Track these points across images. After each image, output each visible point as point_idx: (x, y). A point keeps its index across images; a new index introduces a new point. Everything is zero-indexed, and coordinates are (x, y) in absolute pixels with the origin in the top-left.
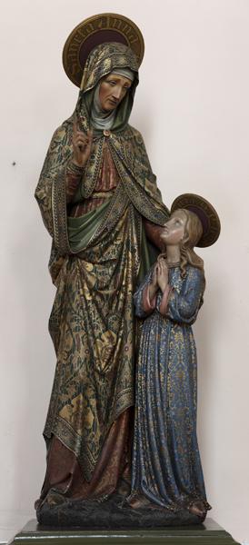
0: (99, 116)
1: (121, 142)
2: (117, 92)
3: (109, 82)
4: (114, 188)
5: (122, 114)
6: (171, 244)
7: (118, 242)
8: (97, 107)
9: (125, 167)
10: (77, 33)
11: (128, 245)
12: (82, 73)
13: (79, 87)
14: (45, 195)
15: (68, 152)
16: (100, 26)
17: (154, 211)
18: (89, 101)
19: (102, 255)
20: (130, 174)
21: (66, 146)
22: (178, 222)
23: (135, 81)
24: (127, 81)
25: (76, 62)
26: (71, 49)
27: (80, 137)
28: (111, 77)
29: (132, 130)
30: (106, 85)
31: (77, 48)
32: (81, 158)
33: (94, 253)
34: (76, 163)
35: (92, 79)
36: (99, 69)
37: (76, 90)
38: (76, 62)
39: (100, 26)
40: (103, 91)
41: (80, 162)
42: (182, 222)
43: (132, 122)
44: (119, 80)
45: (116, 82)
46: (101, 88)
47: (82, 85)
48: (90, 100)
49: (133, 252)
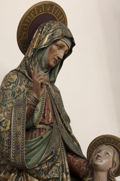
3: (57, 45)
4: (52, 123)
6: (102, 171)
7: (58, 165)
10: (34, 10)
11: (63, 168)
12: (27, 50)
13: (24, 55)
14: (4, 118)
15: (20, 90)
16: (48, 10)
17: (75, 146)
18: (40, 56)
19: (47, 174)
20: (60, 116)
21: (18, 86)
22: (108, 154)
23: (70, 52)
25: (26, 31)
26: (26, 20)
28: (59, 42)
30: (54, 47)
31: (30, 20)
33: (43, 170)
34: (36, 96)
35: (46, 40)
36: (53, 35)
37: (22, 56)
38: (26, 31)
39: (48, 10)
40: (52, 51)
42: (110, 154)
43: (56, 84)
44: (64, 46)
45: (61, 47)
46: (51, 49)
47: (26, 54)
48: (41, 55)
49: (66, 174)
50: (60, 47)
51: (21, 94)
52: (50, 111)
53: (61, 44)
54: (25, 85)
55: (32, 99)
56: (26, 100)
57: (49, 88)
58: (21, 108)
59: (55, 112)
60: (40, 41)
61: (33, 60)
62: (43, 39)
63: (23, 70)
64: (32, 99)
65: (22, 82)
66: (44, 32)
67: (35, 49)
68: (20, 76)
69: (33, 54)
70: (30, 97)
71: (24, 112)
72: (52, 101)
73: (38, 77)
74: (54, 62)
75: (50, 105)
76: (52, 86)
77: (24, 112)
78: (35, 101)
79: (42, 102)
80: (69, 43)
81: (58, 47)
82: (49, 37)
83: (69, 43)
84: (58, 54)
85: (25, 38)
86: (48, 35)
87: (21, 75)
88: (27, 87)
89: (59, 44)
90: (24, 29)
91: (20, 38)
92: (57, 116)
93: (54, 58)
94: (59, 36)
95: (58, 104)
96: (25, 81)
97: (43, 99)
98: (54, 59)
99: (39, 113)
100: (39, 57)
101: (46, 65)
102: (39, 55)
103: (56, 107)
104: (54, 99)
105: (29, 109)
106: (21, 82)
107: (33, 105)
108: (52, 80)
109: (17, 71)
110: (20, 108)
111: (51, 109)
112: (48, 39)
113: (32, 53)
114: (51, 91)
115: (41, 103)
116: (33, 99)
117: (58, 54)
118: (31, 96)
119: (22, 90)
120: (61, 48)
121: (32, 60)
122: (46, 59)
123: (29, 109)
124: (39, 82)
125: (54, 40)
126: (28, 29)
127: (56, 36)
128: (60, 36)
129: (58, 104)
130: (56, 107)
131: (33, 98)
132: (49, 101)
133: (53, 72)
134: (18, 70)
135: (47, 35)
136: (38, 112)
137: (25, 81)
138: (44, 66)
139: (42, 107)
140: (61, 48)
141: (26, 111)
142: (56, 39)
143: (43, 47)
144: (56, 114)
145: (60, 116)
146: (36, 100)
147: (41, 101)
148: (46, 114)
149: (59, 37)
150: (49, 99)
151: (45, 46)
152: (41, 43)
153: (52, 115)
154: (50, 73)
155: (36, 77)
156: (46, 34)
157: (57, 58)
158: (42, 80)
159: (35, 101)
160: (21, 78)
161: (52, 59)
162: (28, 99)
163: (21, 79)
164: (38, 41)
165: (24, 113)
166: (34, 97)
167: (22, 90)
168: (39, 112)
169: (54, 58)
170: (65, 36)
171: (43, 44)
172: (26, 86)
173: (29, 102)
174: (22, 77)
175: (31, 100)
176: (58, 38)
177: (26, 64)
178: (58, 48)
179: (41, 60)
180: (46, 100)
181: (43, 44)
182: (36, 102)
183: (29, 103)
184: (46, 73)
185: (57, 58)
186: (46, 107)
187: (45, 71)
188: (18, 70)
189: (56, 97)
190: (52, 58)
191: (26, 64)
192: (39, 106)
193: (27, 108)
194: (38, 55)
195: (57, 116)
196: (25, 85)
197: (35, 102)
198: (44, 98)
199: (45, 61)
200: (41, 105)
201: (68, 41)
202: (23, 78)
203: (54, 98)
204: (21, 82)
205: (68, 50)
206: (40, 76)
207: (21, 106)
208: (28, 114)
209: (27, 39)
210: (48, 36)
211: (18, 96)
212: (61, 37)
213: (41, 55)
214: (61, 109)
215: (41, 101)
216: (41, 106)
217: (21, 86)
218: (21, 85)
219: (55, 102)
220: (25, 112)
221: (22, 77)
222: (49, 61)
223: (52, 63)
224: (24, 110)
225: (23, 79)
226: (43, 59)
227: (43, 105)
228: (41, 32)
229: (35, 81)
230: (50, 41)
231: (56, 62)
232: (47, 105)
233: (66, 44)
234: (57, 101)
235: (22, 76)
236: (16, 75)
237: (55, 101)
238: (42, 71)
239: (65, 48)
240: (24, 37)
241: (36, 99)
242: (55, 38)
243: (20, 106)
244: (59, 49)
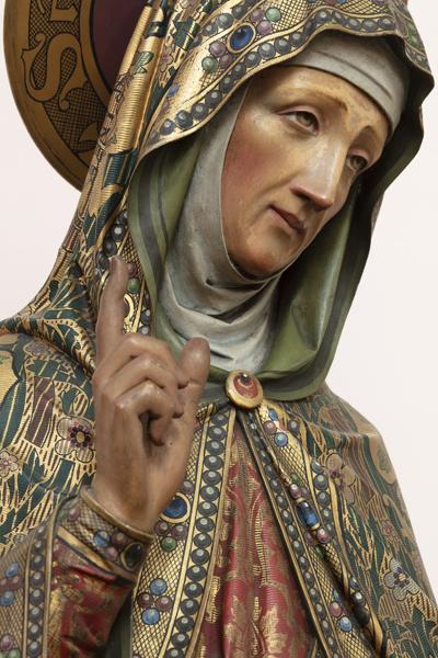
0: (201, 295)
1: (311, 447)
2: (322, 166)
3: (282, 110)
5: (310, 315)
8: (198, 251)
9: (338, 582)
15: (32, 471)
18: (161, 202)
20: (361, 622)
23: (405, 137)
24: (370, 117)
25: (73, 28)
27: (146, 364)
28: (298, 85)
29: (344, 415)
30: (264, 124)
32: (143, 485)
34: (115, 511)
35: (192, 88)
36: (240, 36)
38: (73, 28)
40: (245, 156)
41: (137, 507)
43: (343, 379)
44: (340, 105)
45: (314, 118)
47: (86, 189)
48: (170, 199)
50: (307, 116)
51: (37, 497)
52: (271, 597)
53: (312, 93)
54: (74, 432)
55: (89, 536)
56: (45, 546)
57: (257, 433)
58: (17, 606)
59: (316, 599)
60: (160, 92)
61: (121, 237)
62: (175, 73)
63: (53, 323)
64: (89, 536)
65: (49, 413)
66: (182, 27)
67: (128, 154)
68: (39, 364)
69: (116, 199)
70: (73, 520)
71: (34, 630)
72: (289, 522)
73: (118, 371)
74: (280, 234)
75: (266, 552)
76: (280, 412)
77: (34, 630)
78: (111, 543)
79: (195, 540)
80: (381, 80)
81: (293, 118)
82: (213, 57)
83: (390, 91)
84: (294, 175)
85: (77, 80)
86: (207, 42)
87: (49, 355)
88: (88, 440)
89: (292, 98)
90: (57, 15)
91: (37, 88)
92: (327, 633)
93: (272, 207)
94: (282, 43)
95: (345, 535)
96: (69, 398)
97: (206, 514)
98: (270, 214)
99: (177, 621)
100: (154, 213)
101: (220, 268)
102: (153, 196)
103: (326, 559)
104: (299, 509)
105: (79, 609)
106: (42, 406)
107: (95, 577)
108: (292, 356)
109: (22, 330)
110: (8, 604)
111: (271, 583)
112: (208, 71)
113: (110, 190)
114: (279, 445)
115: (190, 546)
116: (96, 534)
117: (294, 175)
118: (78, 515)
119: (50, 472)
120: (316, 127)
121: (110, 237)
122: (214, 218)
123: (79, 609)
124: (128, 404)
125: (251, 72)
126: (85, 14)
127: (264, 49)
128: (291, 42)
129: (345, 535)
130: (326, 559)
131: (99, 525)
132: (260, 523)
133: (298, 300)
134: (27, 327)
135: (199, 43)
136: (165, 615)
137: (69, 398)
138: (204, 270)
139: (195, 578)
140: (316, 127)
141: (52, 627)
142: (263, 65)
143: (177, 134)
144: (322, 616)
145: (361, 622)
146: (120, 537)
147: (193, 531)
148: (229, 628)
149: (285, 51)
150: (262, 507)
151: (185, 125)
152: (164, 111)
153: (281, 628)
154: (277, 318)
155: (110, 369)
156: (194, 34)
157: (292, 206)
158: (148, 389)
159: (111, 543)
160: (45, 383)
161: (257, 216)
162: (62, 532)
163: (39, 391)
164: (142, 98)
165: (33, 637)
166: (100, 515)
167: (50, 472)
168: (177, 613)
169: (272, 207)
170: (329, 33)
171: (172, 116)
172: (80, 439)
173: (71, 559)
174: (48, 372)
175: (83, 540)
176: (279, 59)
177: (77, 270)
178: (291, 125)
179: (175, 232)
180: (230, 520)
181: (172, 116)
182: (118, 547)
183: (69, 562)
184: (238, 322)
185: (292, 206)
186: (234, 574)
187: (223, 307)
188: (27, 327)
189: (323, 487)
190: (255, 208)
191: (77, 270)
192: (173, 571)
193: (55, 603)
194: (143, 199)
195: (327, 633)
196: (74, 432)
197: (112, 551)
198: (215, 510)
199: (209, 237)
200: (188, 563)
201: (364, 67)
202: (61, 377)
203: (308, 497)
204: (42, 406)
205: (381, 134)
206: (133, 357)
207: (13, 588)
208: (70, 645)
209: (88, 81)
210: (203, 52)
211: (22, 514)
212: (297, 44)
213: (170, 199)
214: (373, 573)
215: (193, 531)
216: (189, 571)
217: (39, 442)
218: (38, 434)
219: (309, 527)
220: (41, 629)
221: (48, 372)
222: (233, 232)
223: (260, 243)
224: (34, 620)
225: (59, 389)
226: (191, 224)
227: (207, 557)
228: (164, 25)
229: (104, 398)
230: (223, 88)
231: (289, 230)
232: (237, 558)
233: (371, 83)
234: (330, 520)
235: (52, 365)
236: (8, 363)
237: (311, 518)
238: (196, 308)
239: (348, 120)
240: (65, 76)
241: (121, 530)
242: (256, 62)
243: (8, 595)
244: (301, 135)
